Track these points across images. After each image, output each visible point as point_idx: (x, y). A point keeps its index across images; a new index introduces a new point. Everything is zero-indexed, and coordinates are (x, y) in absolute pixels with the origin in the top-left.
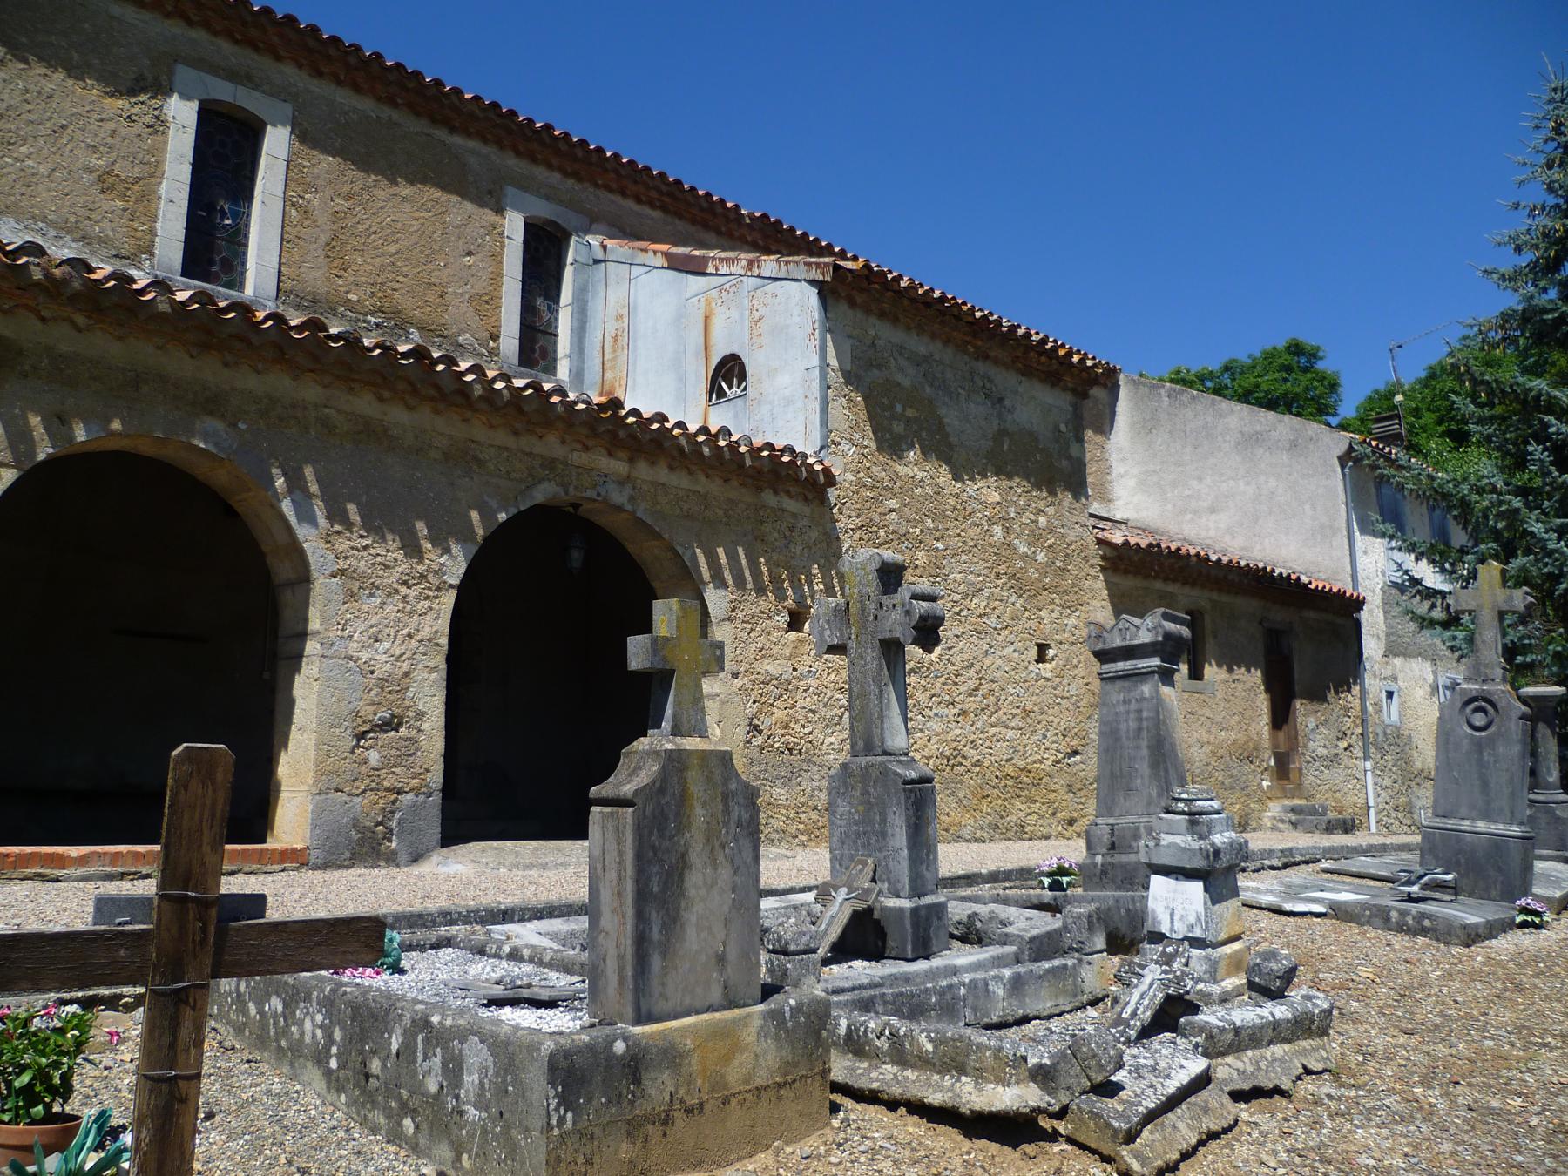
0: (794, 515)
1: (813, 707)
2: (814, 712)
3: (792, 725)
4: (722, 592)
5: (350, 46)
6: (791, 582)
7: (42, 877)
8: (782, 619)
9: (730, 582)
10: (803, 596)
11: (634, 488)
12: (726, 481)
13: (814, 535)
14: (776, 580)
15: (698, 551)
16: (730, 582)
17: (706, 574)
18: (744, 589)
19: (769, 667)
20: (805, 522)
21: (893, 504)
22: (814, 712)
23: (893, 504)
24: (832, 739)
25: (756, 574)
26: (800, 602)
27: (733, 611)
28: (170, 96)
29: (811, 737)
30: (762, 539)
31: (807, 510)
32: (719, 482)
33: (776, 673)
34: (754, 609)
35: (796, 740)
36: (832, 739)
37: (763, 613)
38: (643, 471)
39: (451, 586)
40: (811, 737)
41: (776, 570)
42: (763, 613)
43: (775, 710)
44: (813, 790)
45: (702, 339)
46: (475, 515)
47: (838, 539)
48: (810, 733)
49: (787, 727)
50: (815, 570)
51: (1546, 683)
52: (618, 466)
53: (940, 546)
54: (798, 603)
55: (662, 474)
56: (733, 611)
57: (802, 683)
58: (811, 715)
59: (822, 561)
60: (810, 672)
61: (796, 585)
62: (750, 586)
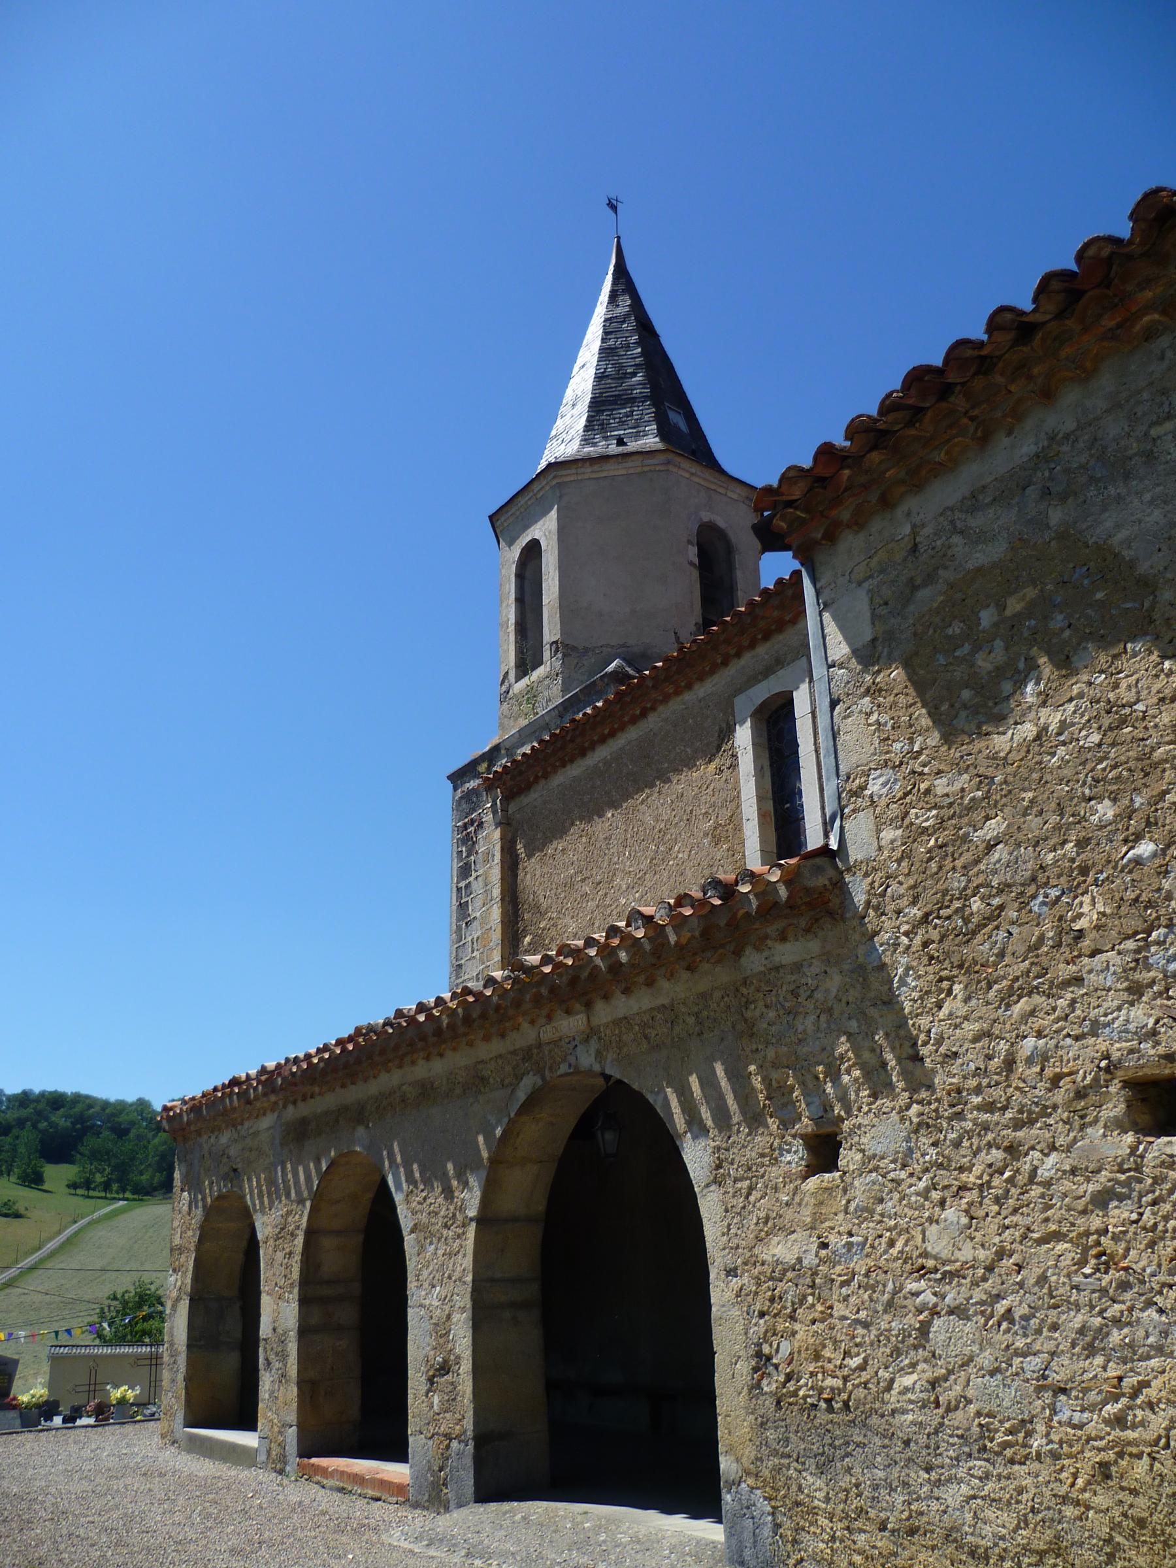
0: (797, 967)
1: (863, 1315)
2: (866, 1325)
3: (827, 1353)
4: (702, 1142)
5: (791, 576)
6: (803, 1084)
7: (341, 1490)
8: (795, 1157)
9: (709, 1123)
10: (827, 1107)
11: (600, 1038)
12: (441, 1055)
13: (834, 983)
14: (778, 1093)
15: (669, 1090)
16: (709, 1123)
17: (679, 1121)
18: (729, 1127)
19: (781, 1250)
20: (817, 967)
21: (994, 827)
22: (866, 1325)
23: (994, 827)
24: (908, 1381)
25: (745, 1096)
26: (824, 1115)
27: (719, 1167)
28: (735, 730)
29: (865, 1376)
30: (750, 1032)
31: (814, 946)
32: (685, 975)
33: (790, 1258)
34: (751, 1154)
35: (838, 1383)
36: (908, 1381)
37: (762, 1155)
38: (604, 1013)
39: (471, 1219)
40: (865, 1376)
41: (775, 1075)
42: (762, 1155)
43: (797, 1326)
44: (876, 1487)
45: (829, 720)
46: (481, 1139)
47: (883, 966)
48: (862, 1368)
49: (817, 1357)
50: (843, 1046)
51: (276, 1173)
52: (571, 1025)
53: (1145, 848)
54: (817, 1121)
55: (623, 1006)
56: (719, 1167)
57: (838, 1269)
58: (860, 1331)
59: (853, 1025)
60: (849, 1246)
61: (813, 1089)
62: (736, 1118)
